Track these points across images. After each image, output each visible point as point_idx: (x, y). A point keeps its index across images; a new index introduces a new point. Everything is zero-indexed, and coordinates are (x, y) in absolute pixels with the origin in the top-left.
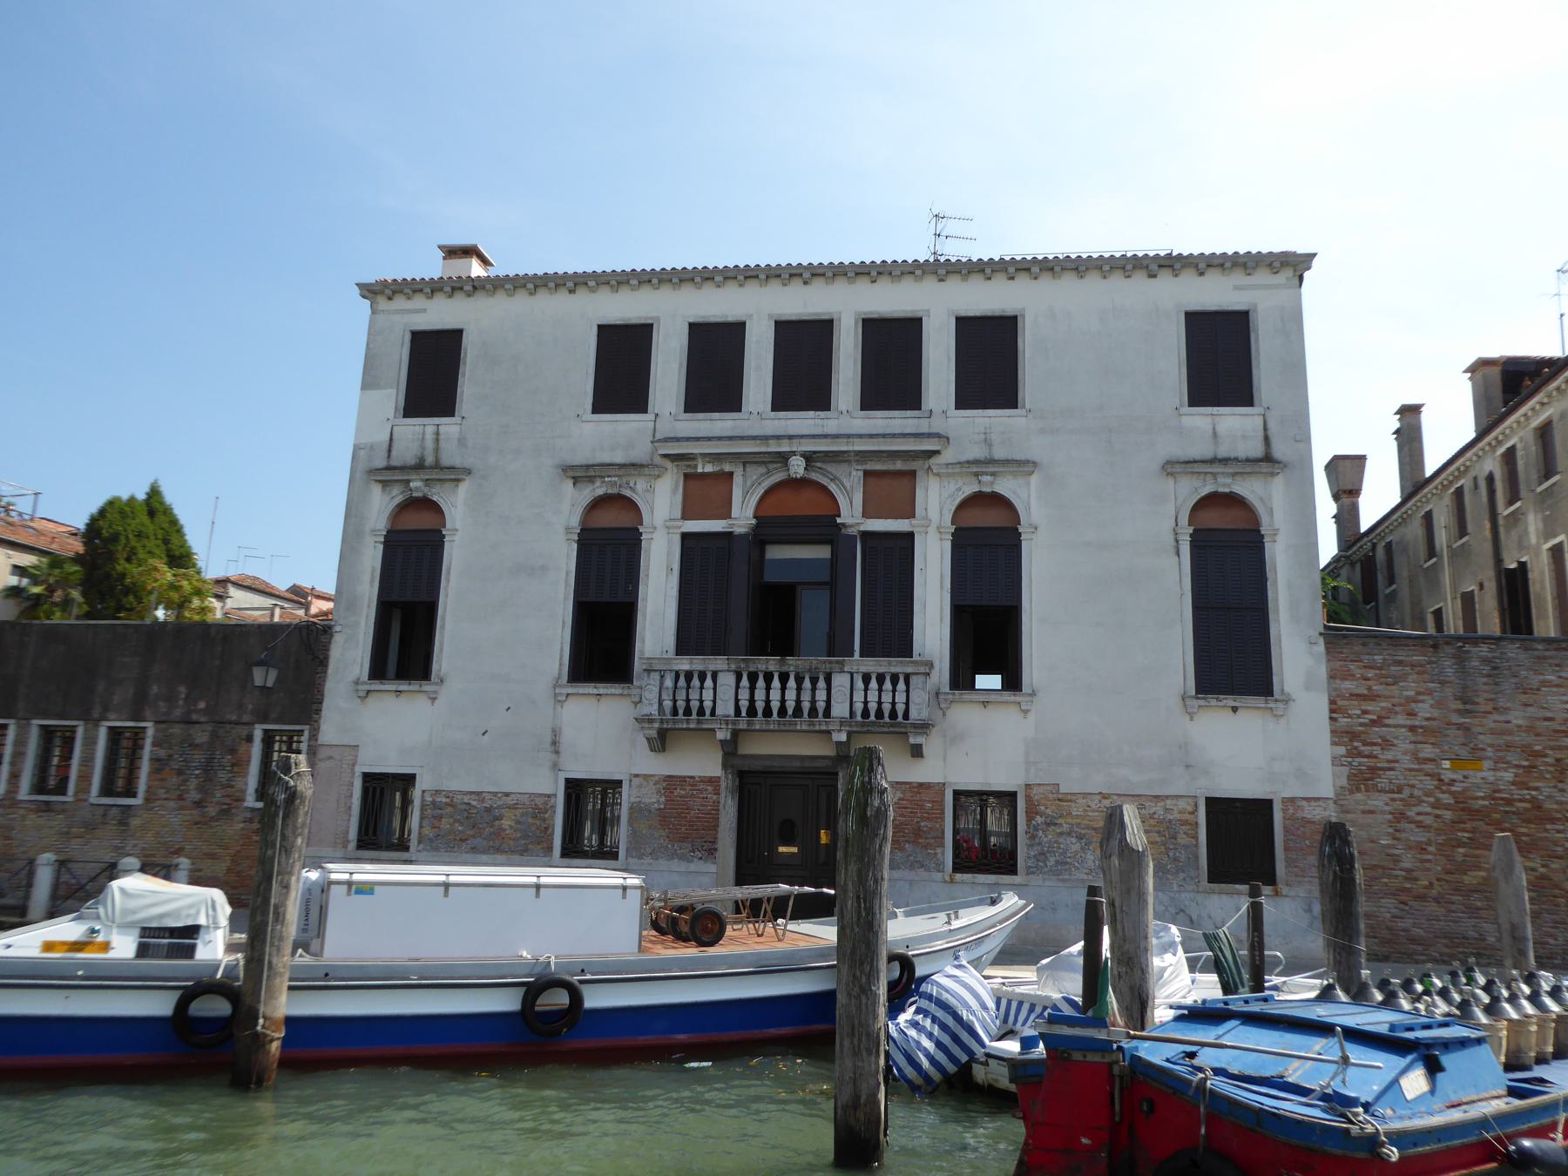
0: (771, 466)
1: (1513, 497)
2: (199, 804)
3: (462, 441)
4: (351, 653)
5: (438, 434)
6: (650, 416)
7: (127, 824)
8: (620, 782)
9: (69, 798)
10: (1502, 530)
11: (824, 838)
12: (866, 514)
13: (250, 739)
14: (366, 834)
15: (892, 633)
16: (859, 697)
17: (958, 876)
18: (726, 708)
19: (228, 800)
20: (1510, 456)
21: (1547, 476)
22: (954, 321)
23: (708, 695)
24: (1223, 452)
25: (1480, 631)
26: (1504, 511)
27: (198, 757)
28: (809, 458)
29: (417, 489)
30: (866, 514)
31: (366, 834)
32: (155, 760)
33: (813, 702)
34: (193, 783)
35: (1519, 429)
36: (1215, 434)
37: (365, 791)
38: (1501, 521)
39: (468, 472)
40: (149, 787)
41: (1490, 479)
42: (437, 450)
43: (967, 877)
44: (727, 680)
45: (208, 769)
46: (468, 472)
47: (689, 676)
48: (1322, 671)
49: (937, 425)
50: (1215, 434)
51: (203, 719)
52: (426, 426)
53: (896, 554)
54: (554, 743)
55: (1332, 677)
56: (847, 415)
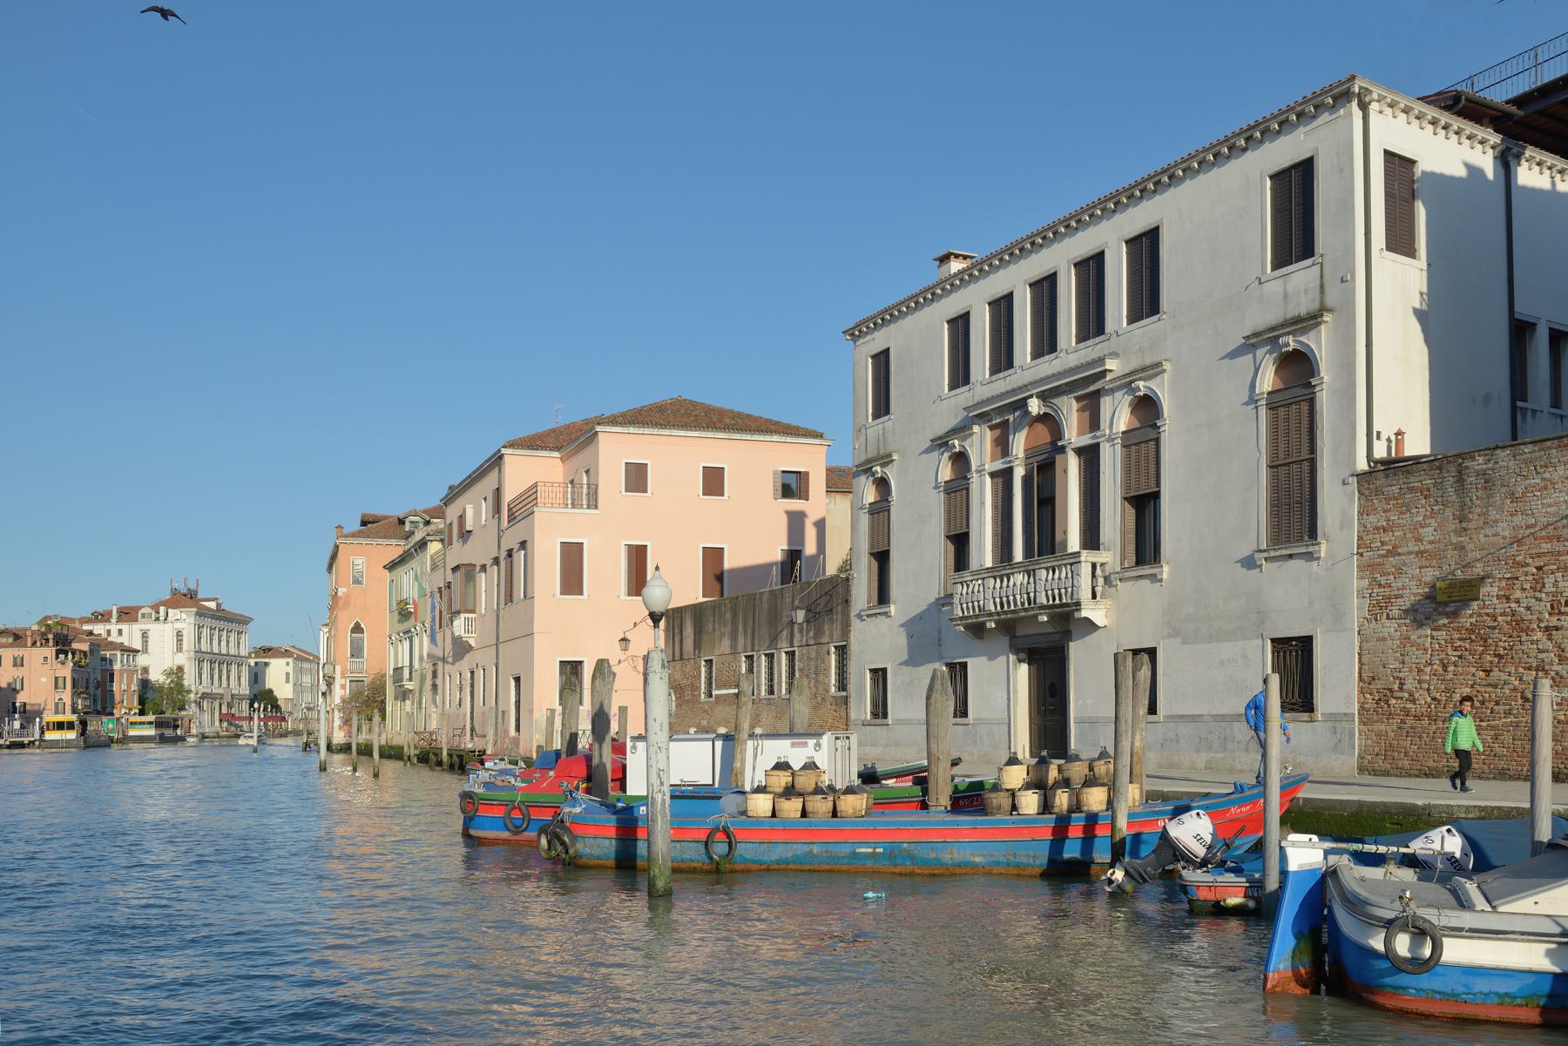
28: (1043, 396)
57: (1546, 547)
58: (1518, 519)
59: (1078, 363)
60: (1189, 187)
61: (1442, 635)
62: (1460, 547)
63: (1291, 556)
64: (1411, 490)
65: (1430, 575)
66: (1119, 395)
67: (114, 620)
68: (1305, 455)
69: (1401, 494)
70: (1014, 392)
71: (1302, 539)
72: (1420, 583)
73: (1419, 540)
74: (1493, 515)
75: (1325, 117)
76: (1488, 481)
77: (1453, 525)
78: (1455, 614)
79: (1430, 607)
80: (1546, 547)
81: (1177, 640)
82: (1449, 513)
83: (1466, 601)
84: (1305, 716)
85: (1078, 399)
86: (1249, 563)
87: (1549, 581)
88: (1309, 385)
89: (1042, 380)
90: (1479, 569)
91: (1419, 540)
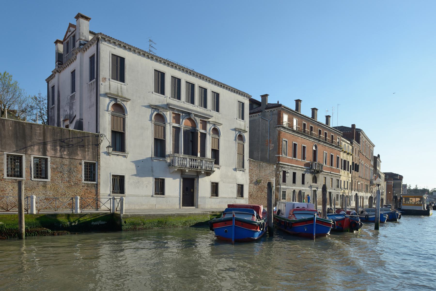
2: (69, 182)
7: (46, 187)
8: (316, 183)
9: (49, 180)
11: (192, 191)
12: (22, 156)
13: (80, 164)
19: (77, 181)
27: (66, 168)
29: (119, 101)
30: (22, 156)
32: (52, 168)
34: (66, 176)
39: (130, 100)
40: (52, 176)
44: (188, 160)
45: (70, 171)
46: (130, 100)
51: (67, 157)
54: (152, 170)
55: (250, 166)
66: (211, 125)
75: (245, 98)
78: (259, 184)
85: (201, 120)
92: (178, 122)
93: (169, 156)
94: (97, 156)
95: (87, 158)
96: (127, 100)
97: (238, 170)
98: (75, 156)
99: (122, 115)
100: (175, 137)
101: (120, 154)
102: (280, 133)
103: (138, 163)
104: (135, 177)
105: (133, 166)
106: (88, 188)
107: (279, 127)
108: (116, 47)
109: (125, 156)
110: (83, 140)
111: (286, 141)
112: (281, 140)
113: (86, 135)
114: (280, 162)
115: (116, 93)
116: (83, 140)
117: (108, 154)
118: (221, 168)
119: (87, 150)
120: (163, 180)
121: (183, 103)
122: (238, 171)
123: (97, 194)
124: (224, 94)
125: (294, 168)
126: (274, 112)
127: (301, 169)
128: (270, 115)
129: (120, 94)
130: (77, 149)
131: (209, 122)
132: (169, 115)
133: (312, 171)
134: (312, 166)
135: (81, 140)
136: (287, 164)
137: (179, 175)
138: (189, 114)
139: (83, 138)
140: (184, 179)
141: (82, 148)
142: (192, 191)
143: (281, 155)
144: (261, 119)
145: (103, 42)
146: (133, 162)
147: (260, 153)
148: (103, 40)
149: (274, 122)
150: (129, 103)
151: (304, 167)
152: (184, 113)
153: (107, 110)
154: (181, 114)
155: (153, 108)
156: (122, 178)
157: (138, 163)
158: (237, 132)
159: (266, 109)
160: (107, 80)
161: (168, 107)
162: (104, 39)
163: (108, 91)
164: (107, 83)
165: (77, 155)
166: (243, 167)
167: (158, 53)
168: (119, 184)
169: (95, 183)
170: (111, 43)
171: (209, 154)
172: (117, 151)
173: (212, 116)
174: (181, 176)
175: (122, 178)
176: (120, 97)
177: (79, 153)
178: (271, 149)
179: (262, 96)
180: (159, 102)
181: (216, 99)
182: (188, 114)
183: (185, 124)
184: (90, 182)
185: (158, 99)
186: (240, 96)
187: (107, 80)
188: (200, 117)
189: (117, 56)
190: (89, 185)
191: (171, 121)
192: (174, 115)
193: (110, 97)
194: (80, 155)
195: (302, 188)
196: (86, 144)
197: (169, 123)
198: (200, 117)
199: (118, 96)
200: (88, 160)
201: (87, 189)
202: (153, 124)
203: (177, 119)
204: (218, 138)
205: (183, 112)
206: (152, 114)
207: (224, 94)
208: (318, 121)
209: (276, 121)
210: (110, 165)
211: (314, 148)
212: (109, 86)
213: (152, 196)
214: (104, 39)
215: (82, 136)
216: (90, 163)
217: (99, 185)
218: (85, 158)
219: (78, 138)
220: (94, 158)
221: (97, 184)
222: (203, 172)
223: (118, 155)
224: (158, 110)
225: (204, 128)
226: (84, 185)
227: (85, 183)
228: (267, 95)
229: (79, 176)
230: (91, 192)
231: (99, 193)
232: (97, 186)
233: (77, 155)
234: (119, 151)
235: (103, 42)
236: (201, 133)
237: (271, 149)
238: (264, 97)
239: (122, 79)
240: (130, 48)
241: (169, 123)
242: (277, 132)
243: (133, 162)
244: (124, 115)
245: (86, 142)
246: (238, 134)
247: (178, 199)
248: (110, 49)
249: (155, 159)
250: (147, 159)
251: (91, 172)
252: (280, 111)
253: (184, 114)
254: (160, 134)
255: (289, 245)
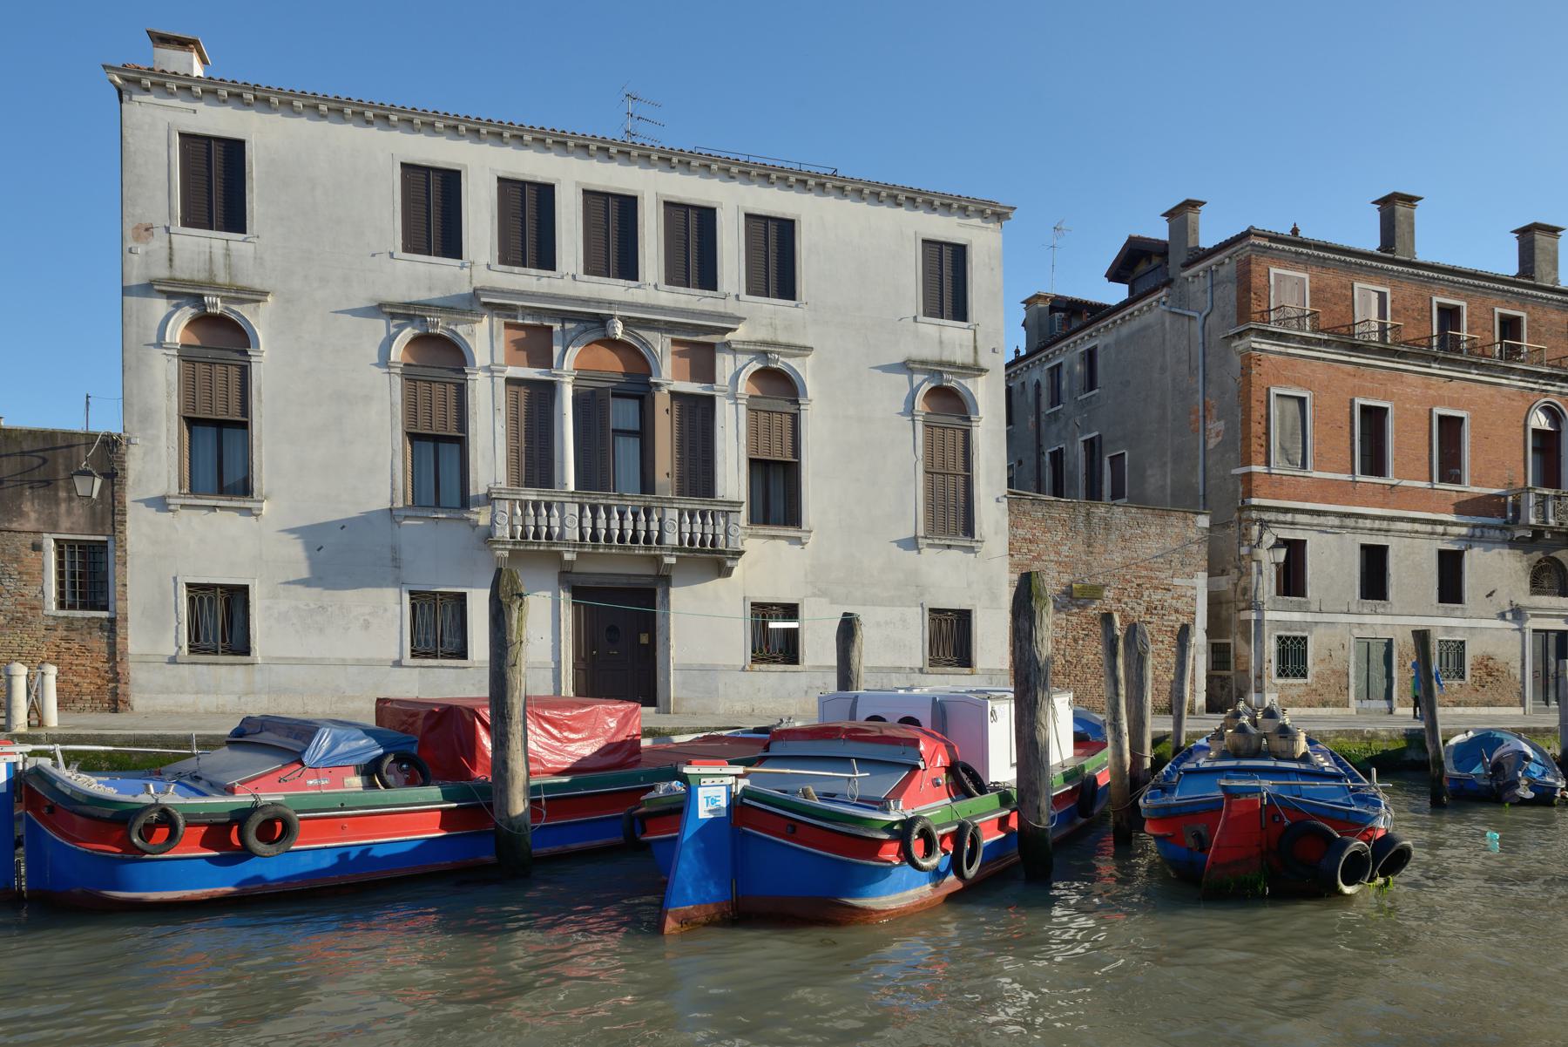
0: (589, 325)
1: (1056, 399)
3: (259, 259)
4: (157, 459)
5: (227, 249)
6: (399, 253)
10: (1043, 424)
11: (644, 639)
13: (37, 547)
14: (197, 639)
15: (698, 474)
16: (686, 528)
17: (756, 667)
18: (573, 534)
19: (20, 608)
20: (1056, 372)
21: (1091, 389)
22: (495, 184)
23: (555, 522)
24: (946, 357)
25: (637, 428)
26: (1047, 410)
28: (627, 322)
31: (197, 639)
33: (648, 531)
35: (1069, 355)
36: (941, 342)
37: (191, 600)
38: (1043, 417)
41: (1038, 385)
42: (229, 267)
43: (764, 666)
47: (536, 505)
48: (1006, 522)
49: (730, 307)
50: (941, 342)
52: (213, 242)
53: (697, 415)
54: (394, 559)
55: (1013, 525)
56: (652, 287)
57: (1144, 573)
58: (1126, 552)
59: (672, 305)
60: (849, 207)
61: (1074, 619)
62: (1088, 564)
63: (949, 547)
64: (1052, 518)
65: (1066, 579)
66: (743, 359)
67: (1226, 673)
68: (960, 469)
69: (1044, 519)
70: (599, 302)
71: (957, 534)
72: (1059, 583)
73: (1058, 553)
74: (1110, 546)
75: (977, 221)
76: (1108, 528)
77: (1081, 548)
78: (1084, 607)
79: (1066, 599)
80: (1144, 573)
81: (823, 600)
82: (1079, 539)
83: (1092, 600)
84: (967, 670)
85: (674, 342)
86: (912, 544)
87: (1146, 593)
88: (968, 419)
89: (642, 306)
90: (1101, 580)
91: (1058, 553)
92: (542, 358)
93: (489, 499)
94: (110, 511)
95: (65, 523)
96: (256, 296)
97: (929, 546)
98: (10, 521)
99: (237, 356)
100: (529, 419)
101: (221, 503)
102: (1248, 359)
103: (316, 538)
104: (300, 589)
105: (296, 551)
106: (73, 635)
107: (1240, 335)
108: (200, 106)
109: (798, 541)
110: (45, 461)
111: (1302, 401)
112: (1257, 394)
113: (60, 443)
114: (1255, 501)
115: (201, 276)
116: (45, 461)
117: (161, 504)
118: (811, 541)
119: (62, 494)
120: (464, 595)
121: (570, 277)
122: (927, 552)
123: (114, 655)
124: (813, 214)
125: (1368, 523)
126: (1223, 271)
127: (1428, 528)
128: (1205, 292)
129: (222, 278)
130: (21, 495)
131: (727, 345)
132: (484, 341)
133: (1518, 534)
134: (1516, 508)
135: (36, 462)
136: (1308, 506)
137: (552, 577)
138: (602, 321)
139: (46, 455)
140: (578, 593)
141: (41, 491)
142: (644, 639)
143: (1257, 469)
144: (1168, 319)
145: (135, 97)
146: (291, 531)
147: (1169, 465)
148: (132, 87)
149: (1223, 317)
150: (810, 360)
151: (1452, 518)
152: (571, 320)
153: (160, 344)
154: (557, 327)
155: (393, 316)
156: (236, 597)
157: (316, 538)
158: (918, 378)
159: (1187, 265)
160: (159, 233)
161: (475, 304)
162: (138, 82)
163: (162, 272)
164: (158, 243)
165: (21, 514)
166: (969, 530)
167: (649, 135)
168: (221, 619)
169: (104, 614)
170: (172, 95)
171: (732, 479)
172: (777, 523)
173: (740, 320)
174: (561, 582)
175: (236, 597)
176: (219, 287)
177: (27, 507)
178: (1212, 443)
179: (1170, 215)
180: (430, 289)
181: (700, 235)
182: (593, 323)
183: (570, 365)
184: (79, 614)
185: (427, 277)
186: (935, 217)
187: (159, 233)
188: (669, 327)
189: (941, 244)
190: (77, 625)
191: (500, 357)
192: (521, 334)
193: (170, 295)
194: (33, 516)
195: (1444, 624)
196: (62, 475)
197: (488, 369)
198: (669, 327)
199: (212, 285)
200: (71, 531)
201: (67, 640)
202: (398, 380)
203: (536, 341)
204: (792, 409)
205: (564, 317)
206: (391, 339)
207: (813, 214)
208: (1421, 257)
209: (1231, 310)
210: (169, 546)
211: (1540, 421)
212: (165, 253)
213: (398, 664)
214: (138, 82)
215: (41, 446)
216: (83, 545)
217: (119, 624)
218: (54, 528)
219: (23, 453)
220: (95, 522)
221: (112, 621)
222: (673, 560)
223: (214, 508)
224: (423, 318)
225: (704, 369)
226: (51, 623)
227: (55, 618)
228: (1192, 205)
229: (31, 591)
230: (85, 649)
231: (124, 652)
232: (111, 627)
233: (21, 514)
234: (785, 524)
235: (135, 97)
236: (675, 395)
237: (1212, 443)
238: (1181, 214)
239: (787, 289)
240: (802, 182)
241: (488, 369)
242: (1237, 360)
243: (291, 531)
244: (796, 402)
245: (61, 468)
246: (926, 387)
247: (549, 675)
248: (170, 116)
249: (406, 517)
250: (367, 519)
251: (90, 576)
252: (1248, 262)
253: (568, 326)
254: (949, 454)
255: (291, 975)
